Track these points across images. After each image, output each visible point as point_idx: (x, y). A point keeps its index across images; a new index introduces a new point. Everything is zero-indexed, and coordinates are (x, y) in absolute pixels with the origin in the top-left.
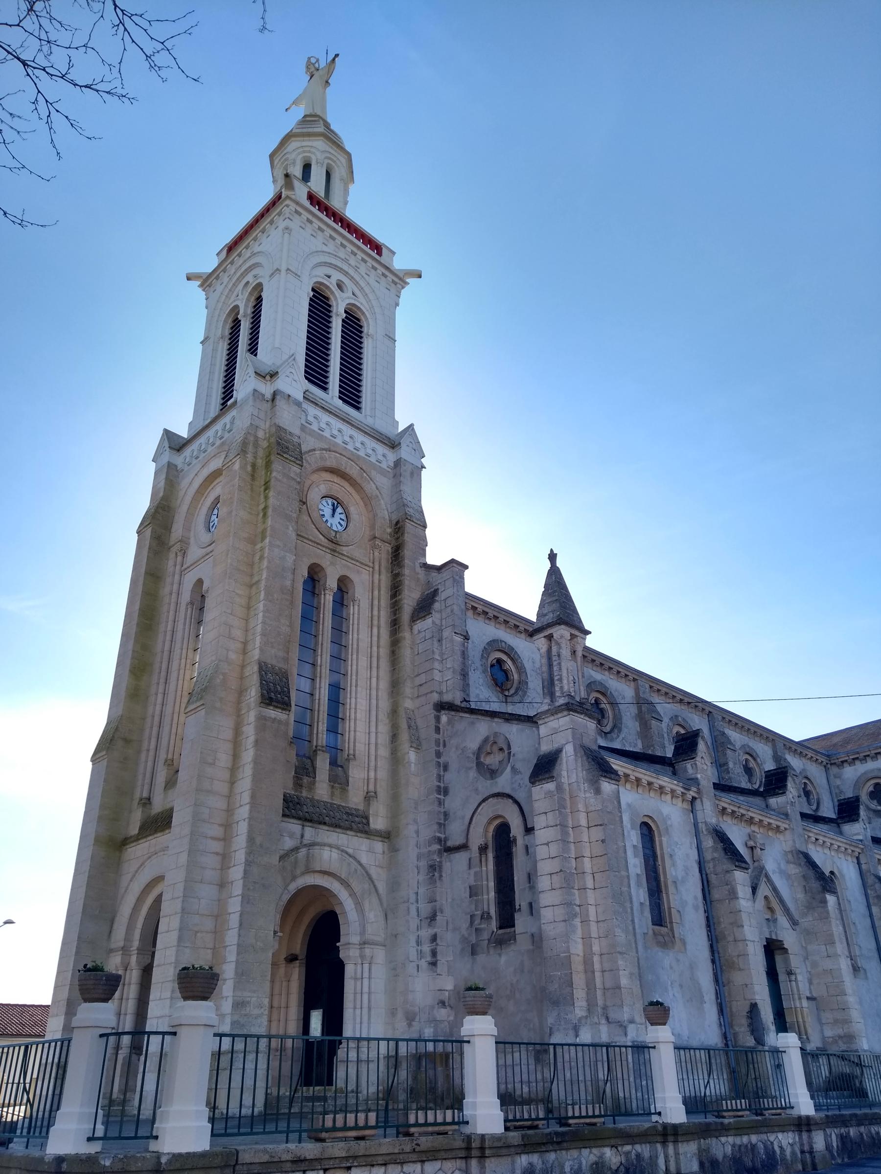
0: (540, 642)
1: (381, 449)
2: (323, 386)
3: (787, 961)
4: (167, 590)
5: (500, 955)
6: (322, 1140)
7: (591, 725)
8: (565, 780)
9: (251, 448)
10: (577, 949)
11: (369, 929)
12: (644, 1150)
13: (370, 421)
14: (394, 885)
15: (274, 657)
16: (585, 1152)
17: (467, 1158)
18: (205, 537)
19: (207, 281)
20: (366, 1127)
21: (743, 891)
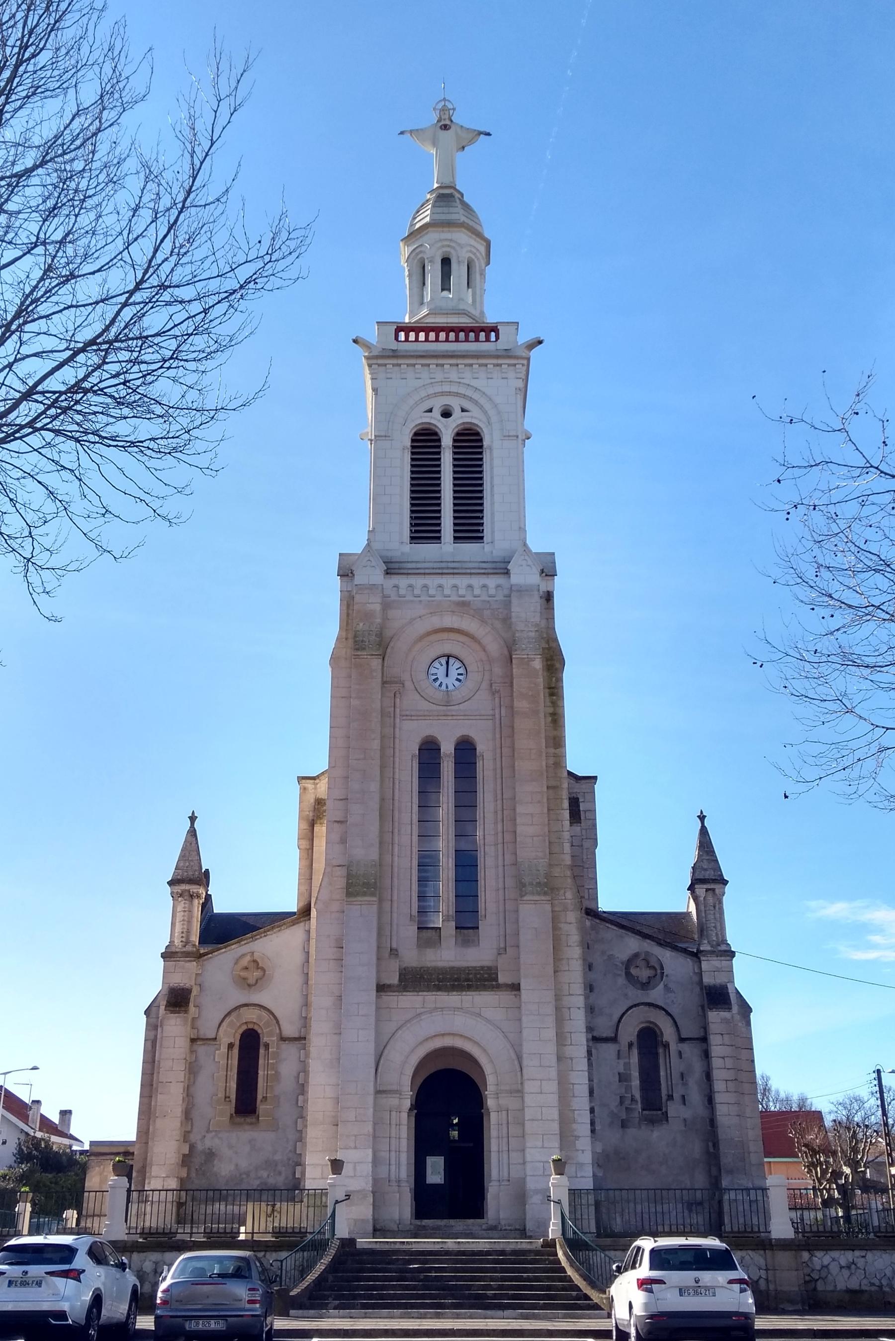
1: (492, 582)
5: (652, 1131)
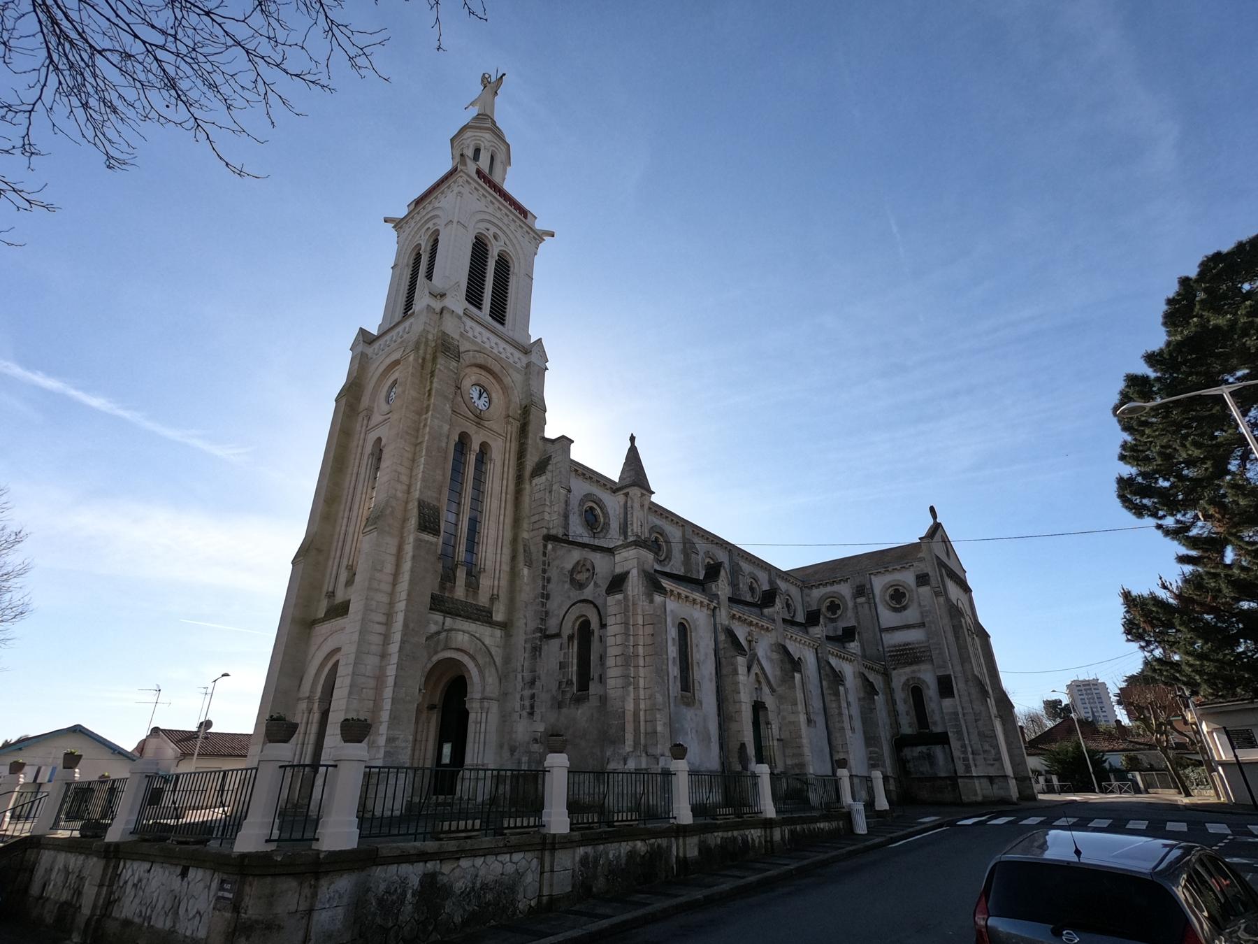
0: (620, 497)
1: (517, 354)
2: (478, 306)
3: (766, 716)
4: (355, 443)
6: (441, 839)
7: (651, 556)
8: (630, 593)
9: (422, 347)
10: (630, 706)
11: (488, 689)
12: (663, 842)
13: (510, 334)
14: (507, 660)
15: (430, 496)
16: (624, 844)
17: (543, 850)
18: (385, 408)
19: (398, 224)
20: (473, 830)
21: (742, 670)
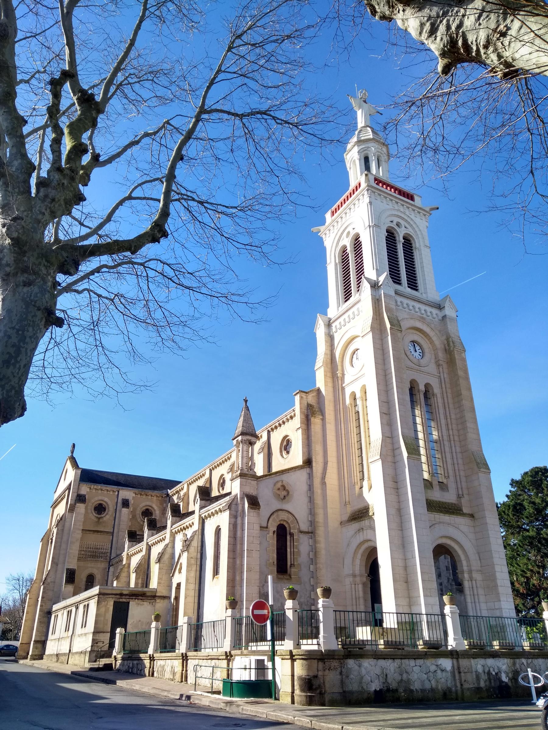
1: (435, 311)
